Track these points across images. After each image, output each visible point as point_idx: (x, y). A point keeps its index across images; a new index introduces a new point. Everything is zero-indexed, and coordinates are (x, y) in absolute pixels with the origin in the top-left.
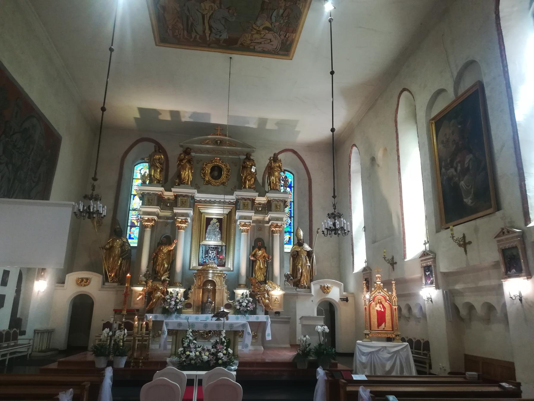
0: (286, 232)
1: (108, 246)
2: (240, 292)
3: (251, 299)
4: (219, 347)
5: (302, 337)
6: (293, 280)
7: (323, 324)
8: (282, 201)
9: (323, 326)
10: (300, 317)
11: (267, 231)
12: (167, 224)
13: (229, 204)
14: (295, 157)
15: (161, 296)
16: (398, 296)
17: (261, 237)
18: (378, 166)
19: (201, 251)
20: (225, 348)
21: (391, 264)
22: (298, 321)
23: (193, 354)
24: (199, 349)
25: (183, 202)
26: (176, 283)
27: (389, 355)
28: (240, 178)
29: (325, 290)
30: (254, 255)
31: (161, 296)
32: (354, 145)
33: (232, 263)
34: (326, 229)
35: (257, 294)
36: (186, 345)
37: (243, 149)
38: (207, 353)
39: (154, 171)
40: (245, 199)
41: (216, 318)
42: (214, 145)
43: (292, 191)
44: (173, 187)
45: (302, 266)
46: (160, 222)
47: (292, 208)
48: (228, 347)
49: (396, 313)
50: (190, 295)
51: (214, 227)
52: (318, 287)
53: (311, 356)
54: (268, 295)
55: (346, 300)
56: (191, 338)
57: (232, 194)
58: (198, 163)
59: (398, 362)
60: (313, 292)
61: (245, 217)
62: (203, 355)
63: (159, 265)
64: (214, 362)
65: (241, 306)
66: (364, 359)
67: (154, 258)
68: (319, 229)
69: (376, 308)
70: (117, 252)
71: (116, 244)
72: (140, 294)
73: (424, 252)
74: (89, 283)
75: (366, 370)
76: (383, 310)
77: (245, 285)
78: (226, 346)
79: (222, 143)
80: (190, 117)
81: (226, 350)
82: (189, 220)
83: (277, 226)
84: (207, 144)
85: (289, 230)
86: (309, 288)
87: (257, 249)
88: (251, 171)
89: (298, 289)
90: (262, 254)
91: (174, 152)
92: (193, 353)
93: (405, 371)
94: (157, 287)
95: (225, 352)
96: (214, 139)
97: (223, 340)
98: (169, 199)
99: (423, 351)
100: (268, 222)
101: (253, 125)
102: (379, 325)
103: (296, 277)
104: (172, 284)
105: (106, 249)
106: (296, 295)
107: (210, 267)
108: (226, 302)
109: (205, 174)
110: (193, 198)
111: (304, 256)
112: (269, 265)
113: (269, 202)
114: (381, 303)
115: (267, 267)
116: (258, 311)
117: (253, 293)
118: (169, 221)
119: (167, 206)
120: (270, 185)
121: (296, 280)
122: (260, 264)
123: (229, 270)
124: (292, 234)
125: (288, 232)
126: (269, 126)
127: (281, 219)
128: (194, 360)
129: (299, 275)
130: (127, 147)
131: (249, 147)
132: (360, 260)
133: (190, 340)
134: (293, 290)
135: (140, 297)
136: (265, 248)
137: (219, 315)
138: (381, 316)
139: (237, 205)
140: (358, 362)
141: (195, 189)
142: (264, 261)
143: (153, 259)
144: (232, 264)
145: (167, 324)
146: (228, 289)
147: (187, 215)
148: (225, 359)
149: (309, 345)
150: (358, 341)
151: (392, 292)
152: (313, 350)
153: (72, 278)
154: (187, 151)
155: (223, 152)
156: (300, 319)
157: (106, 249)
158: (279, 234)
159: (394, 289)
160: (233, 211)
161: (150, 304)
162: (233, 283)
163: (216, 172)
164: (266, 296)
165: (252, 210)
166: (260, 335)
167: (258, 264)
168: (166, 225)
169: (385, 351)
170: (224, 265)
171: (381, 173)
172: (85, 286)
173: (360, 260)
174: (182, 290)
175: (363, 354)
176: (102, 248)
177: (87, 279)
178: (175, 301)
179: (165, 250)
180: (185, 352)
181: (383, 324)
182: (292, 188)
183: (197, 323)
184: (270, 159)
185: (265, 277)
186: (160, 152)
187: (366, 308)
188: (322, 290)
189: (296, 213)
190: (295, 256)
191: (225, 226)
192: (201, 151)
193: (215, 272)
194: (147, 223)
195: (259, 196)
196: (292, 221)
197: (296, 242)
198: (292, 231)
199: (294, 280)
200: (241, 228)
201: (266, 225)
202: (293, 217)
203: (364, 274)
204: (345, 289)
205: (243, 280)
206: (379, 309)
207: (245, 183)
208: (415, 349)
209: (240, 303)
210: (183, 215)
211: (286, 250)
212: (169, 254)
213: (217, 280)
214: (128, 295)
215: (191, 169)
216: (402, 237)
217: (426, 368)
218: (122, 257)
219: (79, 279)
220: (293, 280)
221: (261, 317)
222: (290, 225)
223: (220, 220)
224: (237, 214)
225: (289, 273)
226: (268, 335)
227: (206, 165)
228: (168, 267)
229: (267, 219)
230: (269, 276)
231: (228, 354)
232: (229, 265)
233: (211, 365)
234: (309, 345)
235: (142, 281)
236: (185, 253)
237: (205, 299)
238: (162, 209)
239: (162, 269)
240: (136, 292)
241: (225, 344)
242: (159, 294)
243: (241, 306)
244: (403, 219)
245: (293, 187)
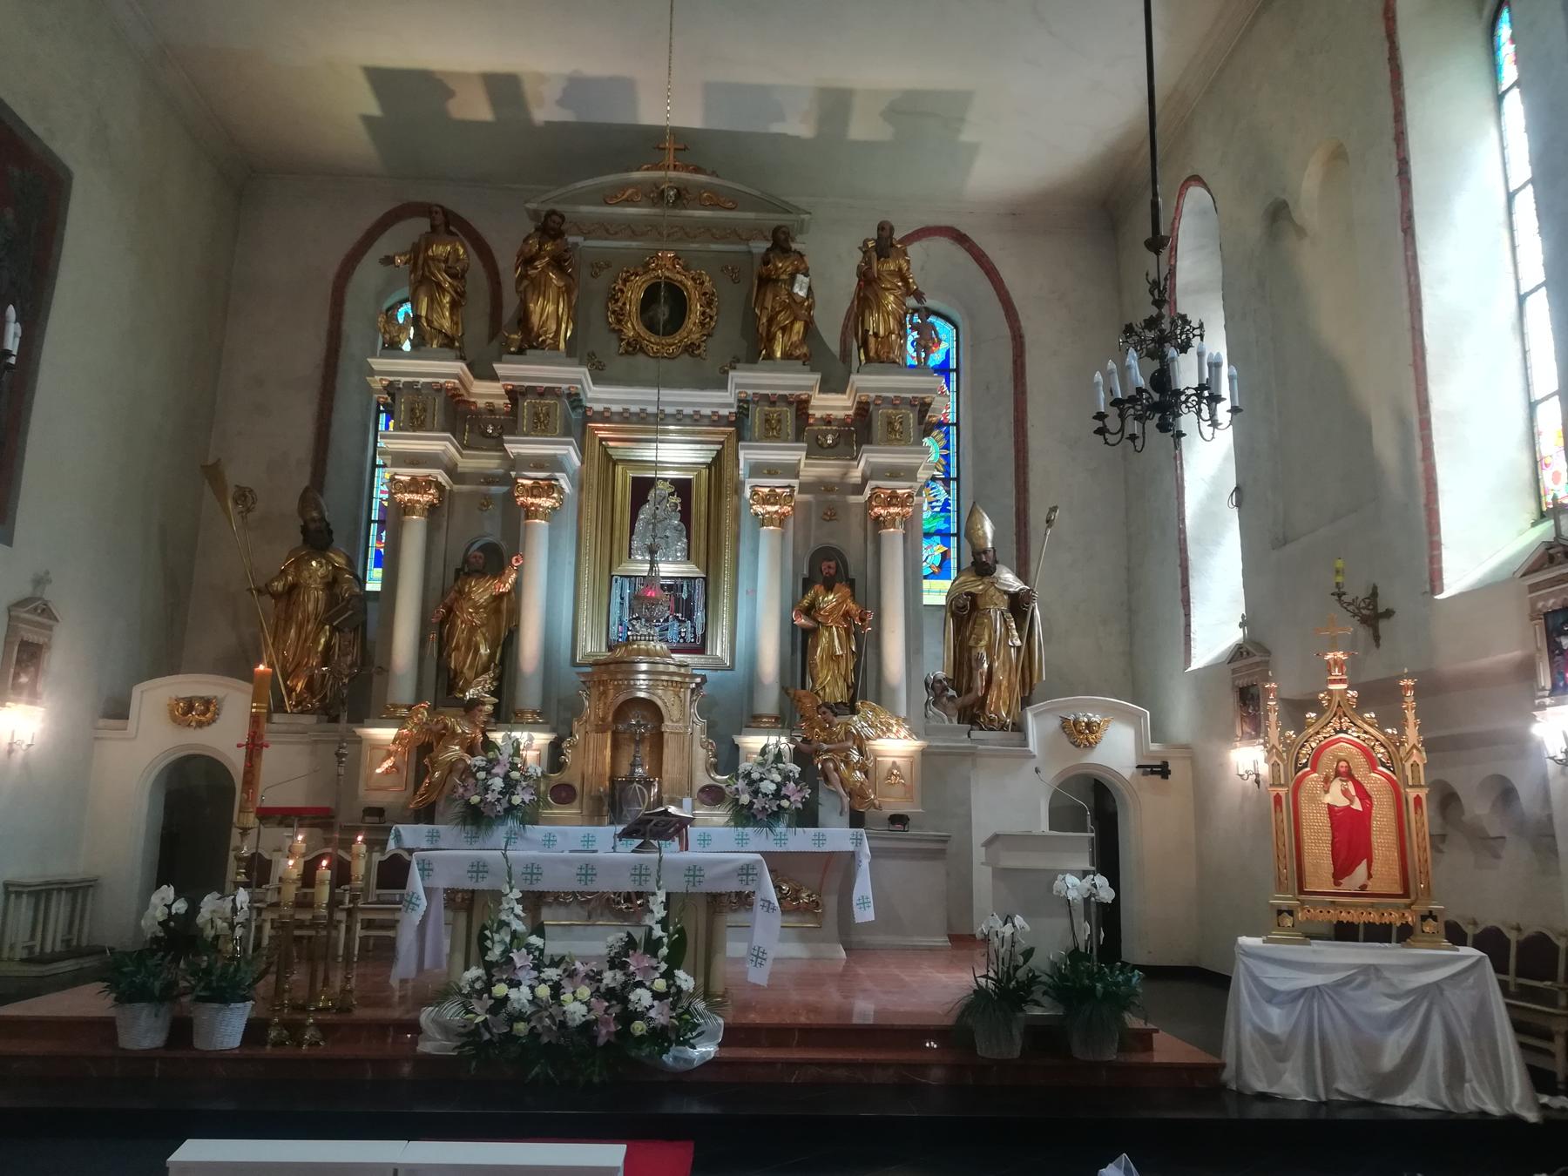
0: (928, 535)
1: (278, 586)
2: (754, 742)
3: (796, 769)
4: (635, 962)
5: (997, 923)
6: (959, 701)
7: (1087, 866)
8: (911, 403)
9: (1085, 874)
10: (983, 840)
11: (855, 522)
12: (487, 499)
13: (714, 423)
14: (961, 255)
15: (462, 760)
16: (1430, 746)
17: (833, 542)
18: (1301, 232)
19: (616, 600)
20: (664, 966)
21: (1365, 620)
22: (979, 854)
23: (520, 997)
24: (551, 973)
25: (536, 414)
26: (523, 712)
27: (1398, 1005)
28: (750, 321)
29: (1080, 734)
30: (810, 610)
31: (462, 760)
32: (1196, 179)
33: (726, 639)
34: (1116, 403)
35: (817, 752)
36: (495, 954)
37: (762, 215)
38: (585, 992)
39: (432, 301)
40: (771, 401)
41: (638, 842)
42: (654, 205)
43: (953, 385)
44: (499, 361)
45: (989, 648)
46: (460, 494)
47: (953, 449)
48: (674, 961)
49: (1422, 822)
50: (568, 757)
51: (662, 504)
52: (1053, 723)
53: (1038, 1004)
54: (861, 753)
55: (1163, 771)
56: (518, 926)
57: (723, 386)
58: (595, 276)
59: (1436, 1039)
60: (1033, 744)
61: (773, 469)
62: (567, 997)
63: (457, 648)
64: (613, 1028)
65: (756, 793)
66: (1277, 1020)
67: (442, 623)
68: (1054, 509)
69: (1328, 799)
70: (311, 607)
71: (306, 574)
72: (389, 754)
73: (1549, 546)
74: (217, 713)
75: (1289, 1065)
76: (1357, 806)
77: (777, 719)
78: (666, 959)
79: (682, 196)
80: (561, 103)
81: (668, 975)
82: (564, 482)
83: (893, 500)
84: (629, 202)
85: (943, 527)
86: (1019, 728)
87: (819, 588)
88: (791, 294)
89: (976, 734)
90: (839, 604)
91: (508, 237)
92: (525, 989)
93: (1469, 1072)
94: (445, 727)
95: (660, 985)
96: (655, 184)
97: (658, 932)
98: (491, 410)
99: (1519, 974)
100: (859, 489)
101: (798, 126)
102: (1342, 869)
103: (969, 690)
104: (505, 714)
105: (276, 596)
106: (970, 755)
107: (639, 652)
108: (702, 779)
109: (620, 316)
110: (575, 400)
111: (997, 612)
112: (866, 644)
113: (863, 411)
114: (1348, 775)
115: (858, 654)
116: (823, 813)
117: (804, 746)
118: (494, 489)
119: (484, 434)
120: (864, 344)
121: (968, 699)
122: (832, 640)
123: (718, 667)
124: (954, 541)
125: (938, 533)
126: (863, 127)
127: (909, 473)
128: (528, 1020)
129: (980, 683)
130: (356, 235)
131: (786, 209)
132: (1216, 621)
133: (514, 934)
134: (958, 737)
135: (388, 764)
136: (851, 584)
137: (665, 828)
138: (1350, 835)
139: (739, 425)
140: (1247, 1029)
141: (581, 364)
142: (847, 631)
143: (438, 625)
144: (727, 645)
145: (426, 869)
146: (711, 730)
147: (555, 464)
148: (660, 1015)
149: (1028, 954)
150: (1245, 941)
151: (1401, 725)
152: (1044, 978)
153: (154, 698)
154: (550, 227)
155: (687, 232)
156: (988, 843)
157: (276, 596)
158: (901, 531)
159: (1410, 715)
160: (728, 451)
161: (422, 790)
162: (729, 714)
163: (665, 306)
164: (855, 756)
165: (797, 440)
166: (831, 902)
167: (824, 641)
168: (483, 507)
169: (1376, 985)
170: (701, 650)
171: (1314, 260)
172: (200, 725)
173: (1216, 621)
174: (542, 739)
175: (1272, 996)
176: (259, 591)
177: (207, 702)
178: (506, 777)
179: (481, 592)
180: (489, 985)
181: (1361, 869)
182: (953, 376)
183: (553, 861)
184: (865, 250)
185: (852, 687)
186: (453, 234)
187: (1278, 799)
188: (1069, 735)
189: (967, 463)
190: (964, 611)
191: (703, 509)
192: (606, 228)
193: (661, 668)
194: (407, 496)
195: (823, 390)
196: (954, 492)
197: (968, 560)
198: (954, 530)
199: (962, 698)
200: (759, 509)
201: (853, 499)
202: (957, 479)
203: (1234, 671)
204: (1158, 732)
205: (769, 702)
206: (1342, 802)
207: (771, 339)
208: (1519, 974)
209: (751, 783)
210: (539, 463)
211: (928, 600)
212: (497, 611)
213: (665, 699)
214: (349, 756)
215: (568, 291)
216: (1422, 500)
217: (1552, 1055)
218: (329, 620)
219: (178, 700)
220: (959, 701)
221: (836, 836)
222: (945, 507)
223: (682, 488)
224: (742, 454)
225: (941, 674)
226: (864, 903)
227: (625, 281)
228: (492, 656)
229: (856, 475)
230: (864, 684)
231: (672, 995)
232: (719, 648)
233: (601, 1041)
234: (1028, 954)
235: (396, 707)
236: (553, 601)
237: (624, 770)
238: (466, 447)
239: (472, 659)
240: (376, 745)
241: (664, 951)
242: (455, 750)
243: (756, 793)
244: (1425, 424)
245: (957, 370)
